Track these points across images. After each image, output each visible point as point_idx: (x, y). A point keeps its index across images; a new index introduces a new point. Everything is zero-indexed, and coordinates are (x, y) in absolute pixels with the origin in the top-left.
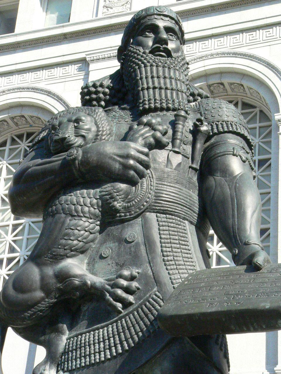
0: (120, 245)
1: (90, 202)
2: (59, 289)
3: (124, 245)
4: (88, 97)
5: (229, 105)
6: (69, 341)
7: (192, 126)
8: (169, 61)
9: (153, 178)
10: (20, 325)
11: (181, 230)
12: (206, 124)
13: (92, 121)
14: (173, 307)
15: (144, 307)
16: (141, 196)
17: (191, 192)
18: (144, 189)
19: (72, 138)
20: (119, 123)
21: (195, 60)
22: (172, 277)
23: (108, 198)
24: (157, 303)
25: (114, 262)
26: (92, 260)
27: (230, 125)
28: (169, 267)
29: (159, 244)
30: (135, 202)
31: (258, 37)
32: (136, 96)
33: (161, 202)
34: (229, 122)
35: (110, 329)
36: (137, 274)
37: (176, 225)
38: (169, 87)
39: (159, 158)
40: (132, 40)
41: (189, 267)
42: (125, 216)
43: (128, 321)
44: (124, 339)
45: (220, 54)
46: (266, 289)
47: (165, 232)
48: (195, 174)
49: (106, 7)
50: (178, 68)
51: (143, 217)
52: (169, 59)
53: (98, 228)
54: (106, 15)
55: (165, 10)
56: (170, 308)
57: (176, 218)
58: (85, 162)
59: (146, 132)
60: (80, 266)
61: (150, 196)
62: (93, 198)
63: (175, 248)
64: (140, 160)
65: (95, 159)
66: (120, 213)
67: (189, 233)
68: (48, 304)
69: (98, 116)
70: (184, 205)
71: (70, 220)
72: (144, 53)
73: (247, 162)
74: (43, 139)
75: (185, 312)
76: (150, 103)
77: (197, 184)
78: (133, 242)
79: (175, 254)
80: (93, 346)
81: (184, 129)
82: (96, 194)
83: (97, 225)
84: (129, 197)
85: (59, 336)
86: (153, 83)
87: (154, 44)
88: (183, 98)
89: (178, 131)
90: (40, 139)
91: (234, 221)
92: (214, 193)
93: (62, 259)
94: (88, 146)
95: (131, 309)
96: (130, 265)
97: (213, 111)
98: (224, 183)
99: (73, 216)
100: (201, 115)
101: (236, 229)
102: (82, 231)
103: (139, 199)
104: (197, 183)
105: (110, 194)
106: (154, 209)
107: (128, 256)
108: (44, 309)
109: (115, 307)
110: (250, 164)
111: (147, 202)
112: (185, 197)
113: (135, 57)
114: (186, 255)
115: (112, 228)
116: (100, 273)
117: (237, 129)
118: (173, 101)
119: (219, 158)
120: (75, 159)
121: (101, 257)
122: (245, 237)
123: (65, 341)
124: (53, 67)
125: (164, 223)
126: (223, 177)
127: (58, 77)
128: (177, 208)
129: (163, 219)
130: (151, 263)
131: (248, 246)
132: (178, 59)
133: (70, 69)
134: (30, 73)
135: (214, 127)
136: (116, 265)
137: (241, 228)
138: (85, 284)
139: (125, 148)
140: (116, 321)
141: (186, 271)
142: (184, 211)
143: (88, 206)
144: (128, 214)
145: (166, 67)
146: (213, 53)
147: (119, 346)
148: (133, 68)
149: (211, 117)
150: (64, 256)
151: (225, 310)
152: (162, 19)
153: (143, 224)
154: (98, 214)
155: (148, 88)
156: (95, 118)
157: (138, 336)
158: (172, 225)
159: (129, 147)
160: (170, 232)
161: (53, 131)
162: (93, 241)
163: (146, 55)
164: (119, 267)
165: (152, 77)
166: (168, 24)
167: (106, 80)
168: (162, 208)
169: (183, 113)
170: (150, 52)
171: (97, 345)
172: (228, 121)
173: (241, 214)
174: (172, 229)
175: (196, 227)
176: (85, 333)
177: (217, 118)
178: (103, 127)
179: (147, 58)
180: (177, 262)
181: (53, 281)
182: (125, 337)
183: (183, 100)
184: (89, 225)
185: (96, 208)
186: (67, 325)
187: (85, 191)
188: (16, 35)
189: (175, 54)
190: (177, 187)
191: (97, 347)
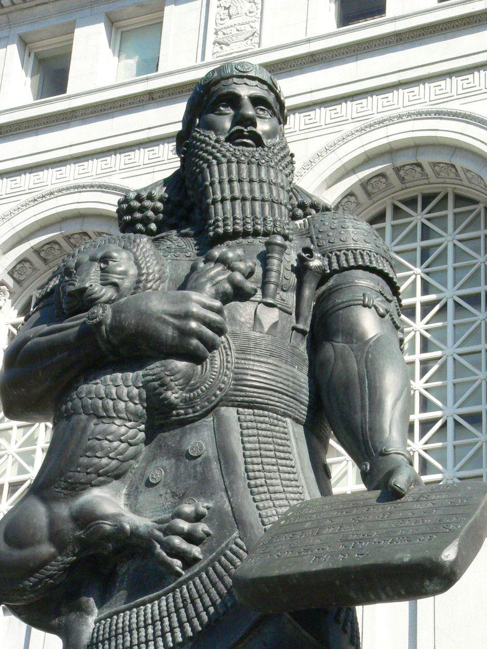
0: (179, 463)
1: (128, 393)
2: (79, 540)
3: (184, 462)
4: (128, 218)
5: (359, 223)
6: (98, 624)
7: (296, 260)
8: (258, 152)
9: (230, 349)
10: (18, 601)
11: (278, 435)
12: (319, 255)
13: (129, 259)
14: (258, 564)
15: (217, 564)
16: (212, 380)
17: (295, 370)
18: (217, 368)
19: (97, 289)
20: (175, 259)
21: (371, 126)
22: (263, 513)
23: (157, 386)
24: (238, 557)
25: (169, 491)
26: (134, 489)
27: (359, 256)
28: (257, 497)
29: (241, 459)
30: (202, 390)
31: (477, 83)
32: (205, 213)
33: (244, 388)
34: (358, 251)
35: (164, 603)
36: (205, 510)
37: (269, 426)
38: (257, 196)
39: (241, 316)
40: (198, 120)
41: (292, 495)
42: (186, 414)
43: (191, 589)
44: (185, 619)
45: (414, 114)
46: (407, 528)
47: (251, 439)
48: (302, 339)
49: (218, 44)
50: (273, 164)
51: (216, 415)
52: (258, 149)
53: (142, 435)
54: (219, 57)
55: (251, 69)
56: (252, 566)
57: (271, 414)
58: (117, 327)
59: (218, 274)
60: (115, 500)
61: (226, 379)
62: (133, 387)
63: (268, 465)
64: (207, 320)
65: (133, 321)
66: (177, 409)
67: (292, 439)
68: (62, 564)
69: (139, 250)
70: (285, 392)
71: (96, 424)
72: (217, 141)
73: (387, 317)
74: (53, 290)
75: (276, 572)
76: (225, 225)
77: (306, 356)
78: (199, 456)
79: (268, 474)
80: (137, 632)
81: (282, 265)
82: (136, 379)
83: (140, 431)
84: (192, 382)
85: (81, 617)
86: (232, 191)
87: (232, 126)
88: (281, 215)
89: (271, 270)
90: (49, 290)
91: (365, 416)
92: (332, 370)
93: (84, 489)
94: (122, 300)
95: (196, 568)
96: (194, 495)
97: (331, 234)
98: (349, 352)
99: (99, 417)
100: (312, 242)
101: (368, 430)
102: (115, 441)
103: (207, 386)
104: (306, 354)
105: (160, 379)
106: (233, 401)
107: (191, 481)
108: (56, 574)
109: (170, 567)
110: (392, 319)
111: (220, 389)
112: (285, 379)
113: (202, 149)
114: (287, 476)
115: (166, 434)
116: (146, 510)
117: (371, 263)
118: (265, 219)
119: (341, 312)
120: (100, 324)
121: (149, 484)
122: (381, 442)
123: (93, 626)
124: (133, 148)
125: (250, 424)
126: (347, 343)
127: (142, 164)
128: (272, 398)
129: (248, 418)
130: (229, 490)
131: (384, 458)
132: (274, 149)
133: (161, 151)
134: (95, 160)
135: (333, 261)
136: (173, 497)
137: (375, 428)
138: (120, 529)
139: (182, 302)
140: (173, 590)
141: (286, 502)
142: (284, 401)
143: (124, 399)
144: (190, 410)
145: (253, 163)
146: (401, 113)
147: (178, 630)
148: (200, 167)
149: (328, 244)
150: (87, 484)
151: (340, 566)
152: (246, 84)
153: (215, 427)
154: (141, 413)
155: (223, 200)
156: (134, 254)
157: (208, 614)
158: (264, 426)
159: (188, 299)
160: (261, 438)
161: (66, 278)
162: (134, 457)
163: (220, 145)
164: (177, 498)
165: (231, 181)
166: (256, 92)
167: (158, 188)
168: (246, 399)
169: (279, 240)
170: (227, 140)
171: (143, 630)
172: (356, 250)
173: (376, 405)
174: (264, 433)
175: (306, 427)
176: (123, 611)
177: (338, 244)
178: (148, 268)
179: (223, 149)
180: (271, 488)
181: (68, 526)
182: (188, 616)
183: (281, 218)
184: (127, 432)
185: (137, 402)
186: (94, 599)
187: (119, 375)
188: (69, 97)
189: (269, 141)
190: (271, 362)
191: (143, 633)
